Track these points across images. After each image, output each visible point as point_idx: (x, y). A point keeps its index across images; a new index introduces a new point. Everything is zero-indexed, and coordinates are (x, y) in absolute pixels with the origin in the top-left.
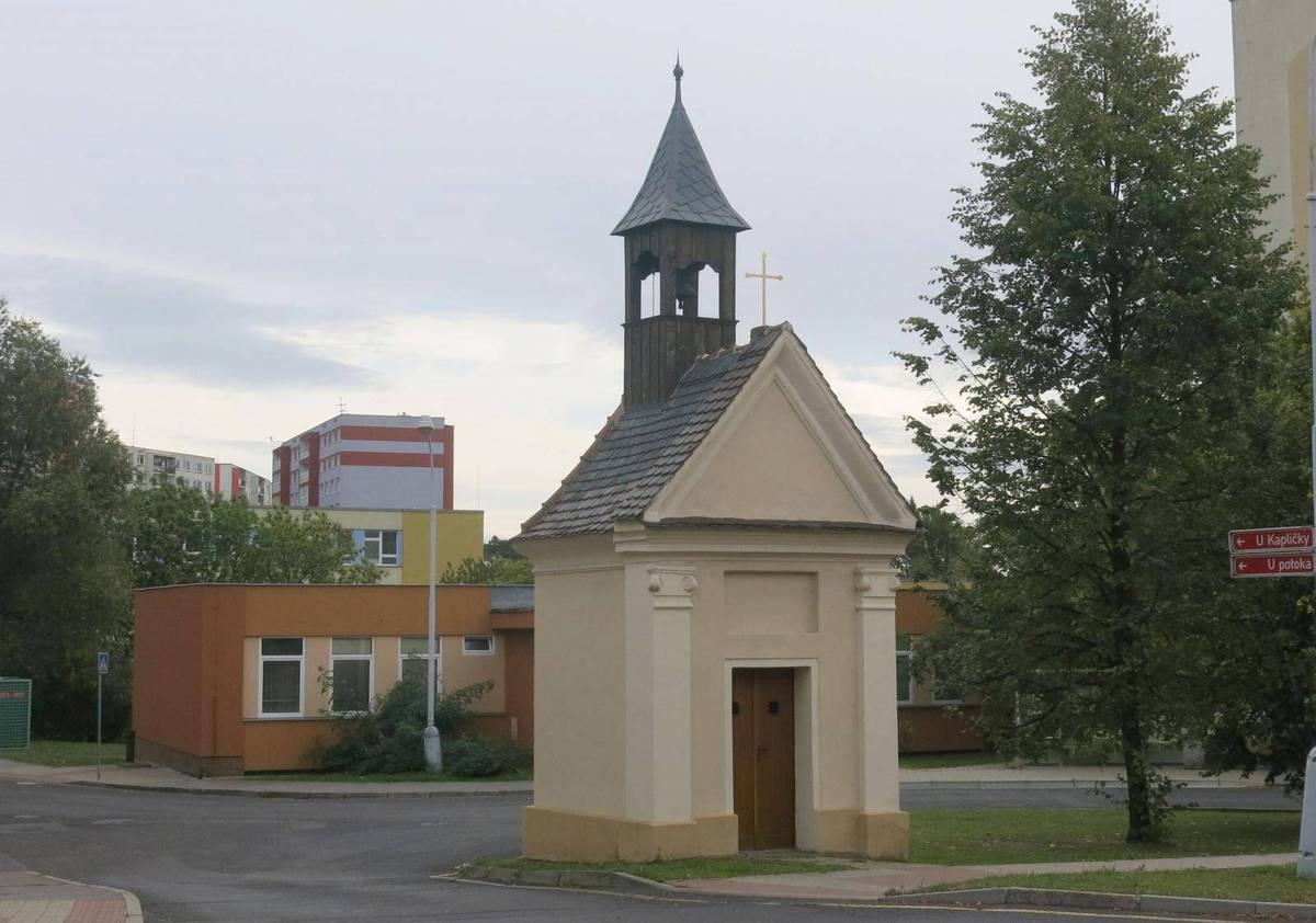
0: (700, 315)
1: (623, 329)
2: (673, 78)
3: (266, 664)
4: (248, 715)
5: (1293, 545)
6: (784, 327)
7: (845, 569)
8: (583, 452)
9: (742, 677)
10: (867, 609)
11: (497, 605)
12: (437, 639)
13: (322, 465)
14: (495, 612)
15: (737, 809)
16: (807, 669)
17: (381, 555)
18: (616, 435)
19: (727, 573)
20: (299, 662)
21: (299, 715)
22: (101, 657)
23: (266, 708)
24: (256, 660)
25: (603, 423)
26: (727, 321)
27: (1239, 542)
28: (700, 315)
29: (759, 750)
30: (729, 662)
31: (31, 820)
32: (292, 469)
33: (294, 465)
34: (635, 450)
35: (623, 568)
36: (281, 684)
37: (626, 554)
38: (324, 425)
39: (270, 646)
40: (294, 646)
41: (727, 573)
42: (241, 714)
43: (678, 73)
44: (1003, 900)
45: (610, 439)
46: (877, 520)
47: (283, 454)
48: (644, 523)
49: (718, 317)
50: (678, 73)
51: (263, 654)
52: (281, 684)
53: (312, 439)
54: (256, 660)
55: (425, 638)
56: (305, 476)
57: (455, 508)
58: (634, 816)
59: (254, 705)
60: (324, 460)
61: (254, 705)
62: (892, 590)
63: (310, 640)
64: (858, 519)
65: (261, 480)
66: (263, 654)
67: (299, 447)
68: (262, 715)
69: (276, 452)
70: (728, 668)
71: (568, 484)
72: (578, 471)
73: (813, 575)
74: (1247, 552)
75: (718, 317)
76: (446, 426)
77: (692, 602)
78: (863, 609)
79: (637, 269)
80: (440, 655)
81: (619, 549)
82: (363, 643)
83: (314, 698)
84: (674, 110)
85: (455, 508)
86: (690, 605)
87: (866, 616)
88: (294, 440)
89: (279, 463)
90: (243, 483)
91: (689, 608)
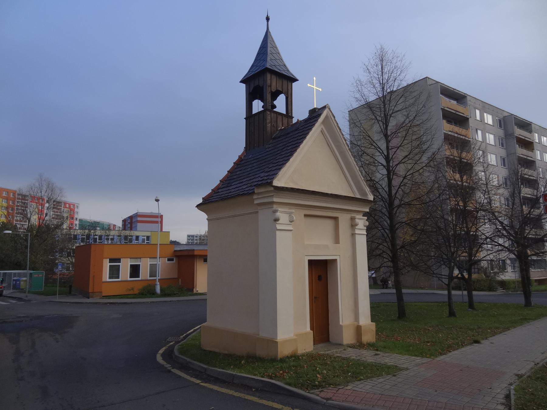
1: (245, 120)
3: (110, 266)
4: (104, 280)
6: (327, 106)
7: (347, 216)
8: (221, 178)
9: (312, 263)
11: (176, 249)
12: (159, 258)
13: (133, 223)
14: (175, 251)
15: (312, 328)
16: (335, 261)
17: (146, 241)
18: (243, 162)
19: (306, 216)
20: (120, 265)
22: (59, 264)
23: (110, 278)
24: (107, 264)
25: (236, 158)
26: (289, 115)
29: (315, 297)
31: (23, 317)
32: (126, 224)
33: (127, 223)
34: (255, 164)
35: (257, 212)
36: (115, 272)
38: (134, 214)
39: (111, 260)
40: (118, 260)
41: (306, 216)
42: (102, 280)
43: (268, 19)
45: (240, 164)
46: (358, 196)
47: (124, 221)
48: (274, 186)
50: (268, 19)
51: (109, 263)
52: (115, 272)
53: (131, 218)
54: (107, 264)
55: (156, 258)
56: (129, 226)
57: (163, 231)
58: (263, 334)
59: (106, 276)
60: (134, 222)
61: (106, 276)
62: (365, 226)
63: (123, 259)
64: (351, 195)
65: (120, 227)
66: (109, 263)
67: (128, 219)
68: (108, 280)
69: (123, 221)
70: (307, 259)
71: (237, 165)
72: (227, 176)
73: (336, 219)
76: (161, 215)
78: (356, 234)
79: (251, 97)
80: (160, 262)
81: (256, 202)
82: (139, 259)
83: (125, 273)
85: (163, 231)
86: (292, 229)
87: (357, 236)
88: (127, 218)
89: (123, 223)
90: (115, 228)
91: (291, 230)
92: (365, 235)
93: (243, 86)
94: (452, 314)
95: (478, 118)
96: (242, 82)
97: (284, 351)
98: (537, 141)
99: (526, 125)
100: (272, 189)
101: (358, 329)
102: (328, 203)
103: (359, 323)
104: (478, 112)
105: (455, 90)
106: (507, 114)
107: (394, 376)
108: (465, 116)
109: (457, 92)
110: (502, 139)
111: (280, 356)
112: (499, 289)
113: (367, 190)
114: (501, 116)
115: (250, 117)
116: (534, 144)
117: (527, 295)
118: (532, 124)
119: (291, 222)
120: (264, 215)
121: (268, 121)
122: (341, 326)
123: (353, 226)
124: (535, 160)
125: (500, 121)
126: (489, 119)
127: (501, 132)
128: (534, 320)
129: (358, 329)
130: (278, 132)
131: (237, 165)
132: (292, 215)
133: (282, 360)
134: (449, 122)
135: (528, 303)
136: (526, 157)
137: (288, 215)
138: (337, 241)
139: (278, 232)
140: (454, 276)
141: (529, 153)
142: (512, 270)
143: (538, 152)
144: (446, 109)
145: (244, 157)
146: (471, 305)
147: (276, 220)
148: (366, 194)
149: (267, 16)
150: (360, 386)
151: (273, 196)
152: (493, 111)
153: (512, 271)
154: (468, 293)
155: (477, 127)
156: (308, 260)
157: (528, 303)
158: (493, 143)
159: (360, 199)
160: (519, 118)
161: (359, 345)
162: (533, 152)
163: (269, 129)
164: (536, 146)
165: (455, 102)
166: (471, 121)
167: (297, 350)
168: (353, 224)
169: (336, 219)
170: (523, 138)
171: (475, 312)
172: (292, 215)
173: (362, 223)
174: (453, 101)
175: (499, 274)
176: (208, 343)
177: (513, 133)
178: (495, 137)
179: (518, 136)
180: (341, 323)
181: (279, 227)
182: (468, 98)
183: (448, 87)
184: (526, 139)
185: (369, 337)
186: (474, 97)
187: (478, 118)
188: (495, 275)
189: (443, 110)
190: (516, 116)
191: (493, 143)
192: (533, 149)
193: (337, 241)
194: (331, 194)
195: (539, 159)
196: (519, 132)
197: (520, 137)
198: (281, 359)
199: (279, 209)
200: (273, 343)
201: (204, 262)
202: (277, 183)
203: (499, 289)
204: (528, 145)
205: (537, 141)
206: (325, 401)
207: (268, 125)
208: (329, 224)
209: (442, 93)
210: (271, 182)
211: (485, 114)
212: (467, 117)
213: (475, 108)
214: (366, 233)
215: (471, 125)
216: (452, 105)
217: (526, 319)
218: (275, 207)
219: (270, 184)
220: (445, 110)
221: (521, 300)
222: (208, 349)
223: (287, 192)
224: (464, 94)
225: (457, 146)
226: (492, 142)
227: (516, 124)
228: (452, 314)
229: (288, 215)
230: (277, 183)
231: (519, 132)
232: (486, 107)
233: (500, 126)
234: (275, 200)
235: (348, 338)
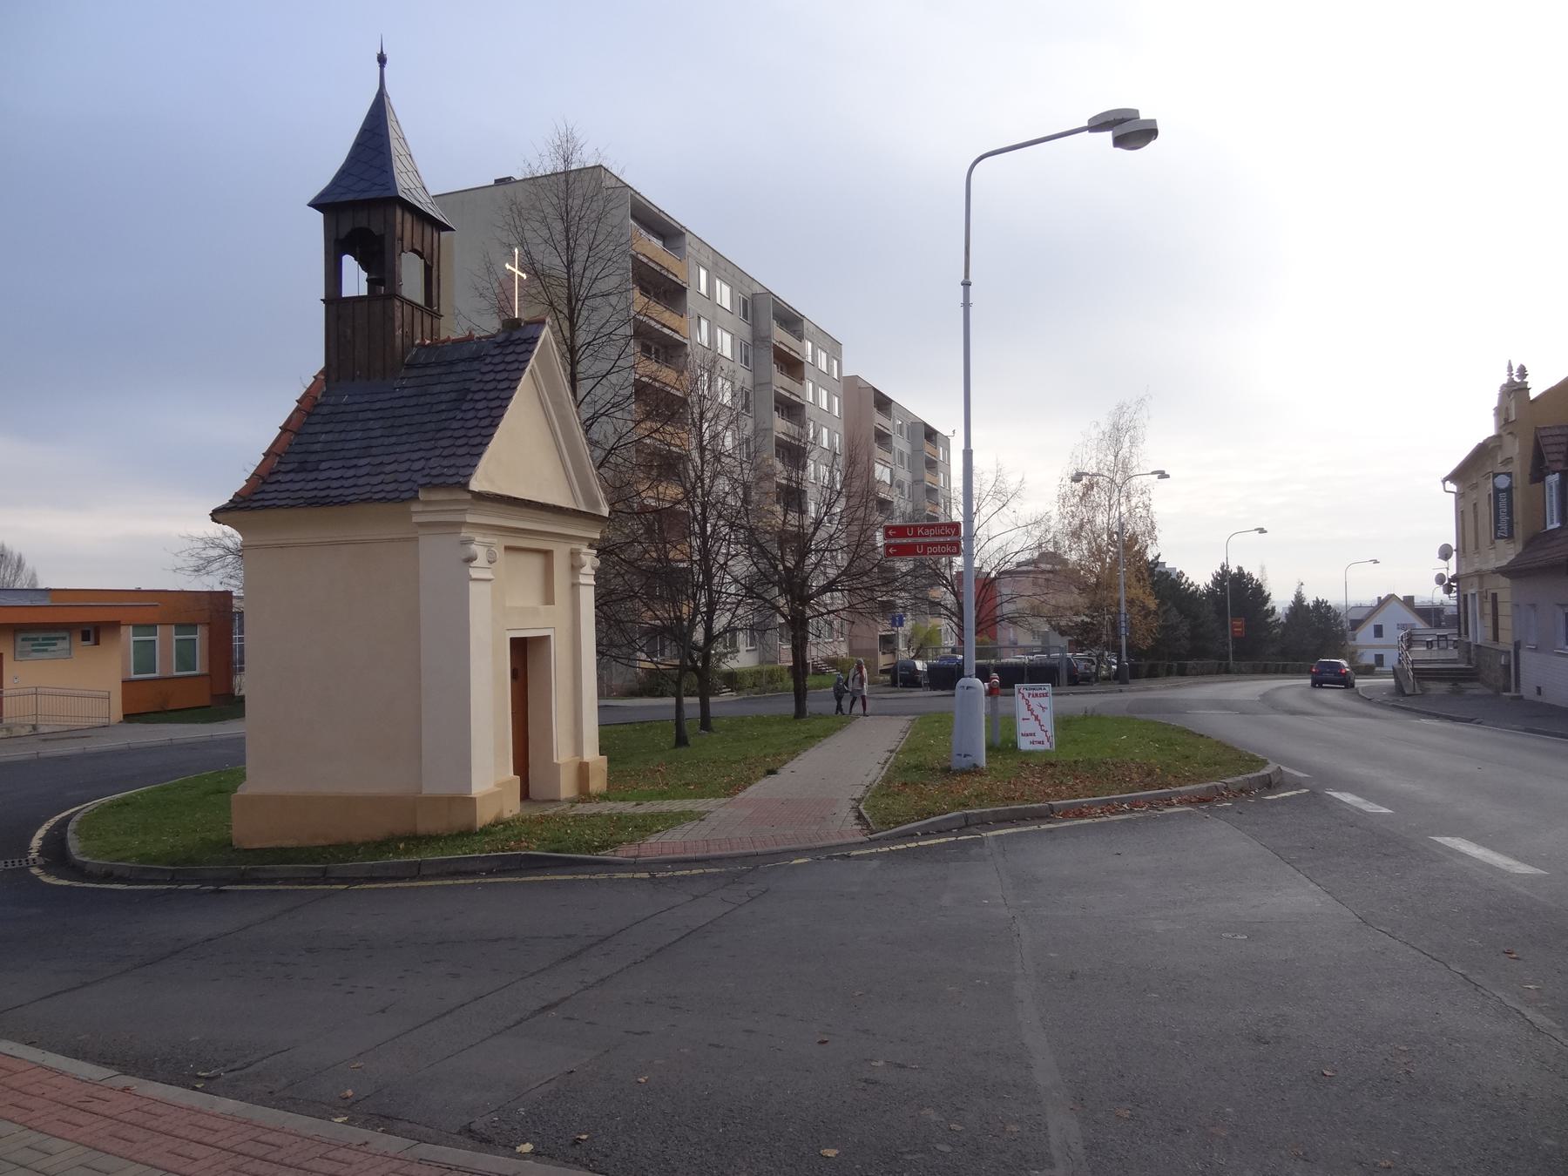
0: (366, 294)
2: (377, 64)
5: (941, 535)
10: (584, 585)
19: (508, 548)
21: (156, 675)
23: (177, 671)
27: (890, 533)
28: (366, 294)
30: (507, 632)
35: (416, 539)
37: (421, 525)
41: (508, 548)
43: (382, 60)
44: (964, 824)
45: (310, 413)
46: (583, 508)
48: (473, 492)
49: (345, 295)
50: (382, 60)
62: (593, 568)
68: (176, 674)
71: (309, 414)
74: (898, 541)
75: (345, 295)
77: (493, 573)
78: (580, 584)
79: (336, 249)
81: (415, 519)
84: (377, 95)
86: (492, 577)
91: (490, 580)
92: (591, 585)
93: (319, 217)
94: (681, 741)
95: (703, 289)
96: (316, 204)
97: (484, 816)
98: (810, 360)
99: (791, 321)
100: (469, 496)
101: (583, 770)
102: (548, 524)
103: (583, 758)
104: (703, 273)
105: (662, 214)
106: (759, 290)
107: (703, 820)
108: (680, 282)
109: (667, 218)
110: (746, 347)
111: (479, 824)
112: (724, 690)
113: (601, 495)
114: (749, 293)
115: (334, 300)
116: (806, 364)
117: (800, 695)
118: (805, 320)
119: (490, 562)
120: (433, 549)
121: (398, 323)
122: (558, 765)
123: (575, 568)
124: (804, 403)
125: (745, 302)
126: (724, 295)
127: (745, 330)
128: (826, 736)
129: (583, 770)
130: (415, 349)
131: (309, 414)
132: (492, 549)
133: (487, 831)
134: (645, 291)
135: (800, 712)
136: (788, 395)
137: (486, 549)
138: (549, 599)
139: (472, 585)
140: (791, 664)
141: (796, 387)
142: (749, 648)
143: (811, 385)
144: (641, 257)
145: (322, 396)
146: (706, 722)
147: (470, 560)
148: (596, 504)
149: (382, 52)
150: (666, 837)
151: (466, 510)
152: (734, 276)
153: (747, 651)
154: (892, 678)
155: (699, 312)
156: (511, 639)
157: (800, 712)
158: (729, 356)
159: (584, 512)
160: (780, 302)
161: (584, 795)
162: (801, 384)
163: (398, 341)
164: (808, 371)
165: (657, 243)
166: (689, 293)
167: (501, 811)
168: (574, 564)
169: (547, 554)
170: (787, 350)
171: (715, 736)
172: (492, 549)
173: (590, 560)
174: (655, 240)
175: (726, 657)
176: (247, 831)
177: (769, 337)
178: (733, 339)
179: (777, 344)
180: (555, 761)
181: (474, 574)
182: (688, 237)
183: (647, 204)
184: (792, 353)
185: (598, 783)
186: (699, 237)
187: (703, 289)
188: (719, 660)
189: (635, 259)
190: (777, 297)
191: (729, 356)
192: (803, 379)
193: (549, 599)
194: (554, 506)
195: (811, 400)
196: (780, 336)
197: (782, 346)
198: (481, 830)
199: (477, 539)
200: (471, 802)
201: (83, 640)
202: (476, 484)
203: (724, 690)
204: (792, 366)
205: (810, 360)
206: (634, 859)
207: (397, 333)
208: (536, 562)
209: (634, 217)
210: (466, 484)
211: (718, 282)
212: (684, 285)
213: (699, 264)
214: (595, 583)
215: (690, 304)
216: (652, 246)
217: (812, 737)
218: (465, 533)
219: (464, 486)
220: (638, 259)
221: (789, 707)
222: (256, 846)
223: (489, 504)
224: (679, 227)
225: (657, 351)
226: (727, 353)
227: (776, 316)
228: (681, 741)
229: (486, 549)
230: (476, 484)
231: (780, 336)
232: (722, 267)
233: (745, 316)
234: (470, 518)
235: (567, 788)
